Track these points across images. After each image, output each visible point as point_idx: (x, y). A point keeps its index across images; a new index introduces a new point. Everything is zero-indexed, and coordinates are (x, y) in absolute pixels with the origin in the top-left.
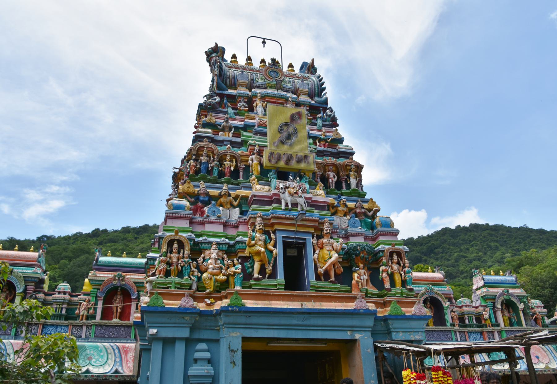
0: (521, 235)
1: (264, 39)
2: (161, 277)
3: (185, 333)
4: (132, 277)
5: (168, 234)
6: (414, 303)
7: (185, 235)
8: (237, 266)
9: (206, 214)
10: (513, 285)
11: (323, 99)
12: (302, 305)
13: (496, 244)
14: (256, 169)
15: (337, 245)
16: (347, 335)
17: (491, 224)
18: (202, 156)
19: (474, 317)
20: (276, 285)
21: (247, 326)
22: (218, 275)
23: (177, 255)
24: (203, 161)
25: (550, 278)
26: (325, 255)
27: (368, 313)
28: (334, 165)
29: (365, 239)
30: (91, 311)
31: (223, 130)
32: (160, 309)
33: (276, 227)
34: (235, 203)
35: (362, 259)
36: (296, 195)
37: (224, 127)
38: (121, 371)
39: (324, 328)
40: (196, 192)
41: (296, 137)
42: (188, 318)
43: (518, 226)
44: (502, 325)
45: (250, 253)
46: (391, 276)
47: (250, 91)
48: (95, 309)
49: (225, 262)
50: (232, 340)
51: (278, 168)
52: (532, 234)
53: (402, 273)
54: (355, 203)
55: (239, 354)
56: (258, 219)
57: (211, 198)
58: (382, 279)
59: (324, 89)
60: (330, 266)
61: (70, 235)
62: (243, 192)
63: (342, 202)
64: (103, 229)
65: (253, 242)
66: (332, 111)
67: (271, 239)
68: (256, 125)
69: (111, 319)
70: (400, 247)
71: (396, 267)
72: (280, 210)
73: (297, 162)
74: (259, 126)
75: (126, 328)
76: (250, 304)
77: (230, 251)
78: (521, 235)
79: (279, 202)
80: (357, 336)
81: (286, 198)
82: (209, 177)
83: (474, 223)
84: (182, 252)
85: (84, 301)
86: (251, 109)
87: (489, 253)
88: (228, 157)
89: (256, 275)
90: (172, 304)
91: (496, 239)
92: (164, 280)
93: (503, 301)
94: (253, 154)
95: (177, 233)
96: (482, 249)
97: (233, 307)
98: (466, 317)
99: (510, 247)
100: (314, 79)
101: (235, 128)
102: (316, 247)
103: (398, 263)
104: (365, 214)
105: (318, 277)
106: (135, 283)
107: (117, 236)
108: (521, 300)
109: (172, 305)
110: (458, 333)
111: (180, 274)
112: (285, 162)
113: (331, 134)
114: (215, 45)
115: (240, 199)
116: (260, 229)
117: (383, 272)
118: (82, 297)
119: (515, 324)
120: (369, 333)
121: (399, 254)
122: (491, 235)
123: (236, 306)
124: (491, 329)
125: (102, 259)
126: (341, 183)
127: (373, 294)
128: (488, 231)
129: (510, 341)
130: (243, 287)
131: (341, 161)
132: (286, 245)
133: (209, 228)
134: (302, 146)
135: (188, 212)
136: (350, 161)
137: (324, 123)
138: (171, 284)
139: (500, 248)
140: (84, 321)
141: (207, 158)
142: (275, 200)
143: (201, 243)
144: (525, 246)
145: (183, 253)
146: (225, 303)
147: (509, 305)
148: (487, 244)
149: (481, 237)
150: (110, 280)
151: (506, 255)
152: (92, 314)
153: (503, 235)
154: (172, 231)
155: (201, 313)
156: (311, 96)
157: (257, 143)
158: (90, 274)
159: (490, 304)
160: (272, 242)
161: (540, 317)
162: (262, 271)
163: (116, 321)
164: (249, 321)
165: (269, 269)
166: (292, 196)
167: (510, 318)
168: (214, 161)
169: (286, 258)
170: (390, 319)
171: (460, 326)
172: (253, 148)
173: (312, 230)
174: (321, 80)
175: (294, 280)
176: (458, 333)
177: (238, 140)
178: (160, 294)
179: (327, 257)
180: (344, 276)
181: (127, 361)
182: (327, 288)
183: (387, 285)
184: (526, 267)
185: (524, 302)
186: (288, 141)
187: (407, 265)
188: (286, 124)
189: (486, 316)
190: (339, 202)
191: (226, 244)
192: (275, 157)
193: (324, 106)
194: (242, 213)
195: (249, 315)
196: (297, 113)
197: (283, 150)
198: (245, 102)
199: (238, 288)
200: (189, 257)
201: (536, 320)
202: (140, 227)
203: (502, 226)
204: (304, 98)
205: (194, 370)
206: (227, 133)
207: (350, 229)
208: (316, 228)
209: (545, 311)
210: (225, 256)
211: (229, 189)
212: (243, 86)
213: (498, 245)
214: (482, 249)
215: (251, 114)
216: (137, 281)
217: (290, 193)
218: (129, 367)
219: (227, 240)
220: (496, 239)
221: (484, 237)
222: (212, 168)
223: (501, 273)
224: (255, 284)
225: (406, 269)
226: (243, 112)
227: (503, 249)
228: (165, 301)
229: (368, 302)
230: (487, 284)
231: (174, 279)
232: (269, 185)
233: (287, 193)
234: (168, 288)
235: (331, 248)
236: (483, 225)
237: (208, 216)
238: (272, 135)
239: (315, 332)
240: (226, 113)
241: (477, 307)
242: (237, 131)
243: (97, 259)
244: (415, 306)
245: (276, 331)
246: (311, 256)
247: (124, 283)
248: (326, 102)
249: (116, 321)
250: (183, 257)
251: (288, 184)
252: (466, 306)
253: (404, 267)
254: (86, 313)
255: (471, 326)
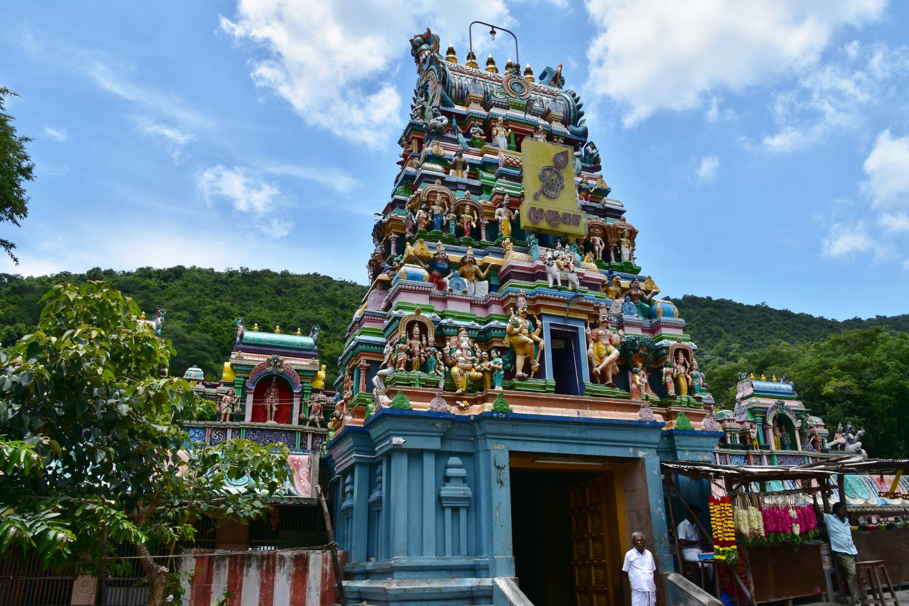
0: (757, 318)
1: (493, 27)
2: (402, 371)
3: (436, 444)
4: (292, 362)
5: (407, 313)
6: (703, 416)
7: (428, 315)
8: (496, 360)
9: (449, 288)
10: (787, 396)
11: (580, 129)
12: (578, 413)
13: (720, 328)
14: (506, 228)
15: (616, 337)
16: (629, 453)
17: (715, 298)
18: (434, 204)
19: (738, 436)
20: (544, 387)
21: (513, 437)
22: (470, 370)
23: (419, 342)
24: (436, 213)
25: (807, 385)
26: (600, 350)
27: (655, 426)
28: (602, 227)
29: (643, 331)
30: (237, 409)
31: (454, 167)
32: (406, 412)
33: (543, 311)
34: (483, 275)
35: (641, 355)
36: (567, 269)
37: (456, 163)
38: (295, 492)
39: (602, 443)
40: (432, 256)
41: (562, 187)
42: (439, 425)
43: (753, 303)
44: (773, 448)
45: (511, 344)
46: (676, 380)
47: (487, 110)
48: (243, 407)
49: (478, 354)
50: (499, 453)
51: (540, 229)
52: (772, 318)
53: (689, 376)
54: (629, 282)
55: (506, 473)
56: (521, 299)
57: (453, 266)
58: (666, 383)
59: (582, 114)
60: (607, 365)
61: (49, 276)
62: (492, 260)
63: (614, 279)
64: (107, 268)
65: (516, 330)
66: (594, 148)
67: (535, 326)
68: (501, 164)
69: (265, 421)
70: (687, 344)
71: (682, 369)
72: (545, 288)
73: (565, 223)
74: (504, 166)
75: (289, 434)
76: (518, 409)
77: (483, 339)
78: (757, 318)
79: (544, 277)
80: (641, 454)
81: (554, 271)
82: (445, 235)
83: (690, 294)
84: (424, 338)
85: (227, 394)
86: (490, 138)
87: (707, 341)
88: (468, 208)
89: (519, 373)
90: (421, 406)
91: (719, 320)
92: (404, 375)
93: (775, 417)
94: (501, 206)
95: (418, 312)
96: (698, 334)
97: (498, 413)
98: (729, 435)
99: (740, 335)
100: (568, 98)
101: (471, 165)
102: (590, 339)
103: (685, 365)
104: (641, 298)
105: (593, 378)
106: (297, 370)
107: (133, 282)
108: (798, 417)
109: (420, 407)
110: (717, 455)
111: (424, 367)
112: (549, 222)
113: (594, 182)
114: (426, 31)
115: (490, 269)
116: (524, 313)
117: (667, 373)
118: (222, 388)
119: (788, 446)
120: (655, 451)
121: (686, 352)
122: (714, 315)
123: (502, 412)
124: (757, 451)
125: (248, 335)
126: (609, 253)
127: (654, 402)
128: (709, 309)
129: (823, 466)
130: (504, 388)
131: (610, 222)
132: (554, 335)
133: (452, 306)
134: (568, 202)
135: (427, 283)
136: (622, 223)
137: (584, 164)
138: (414, 380)
139: (725, 334)
140: (228, 422)
141: (441, 208)
142: (537, 274)
143: (446, 326)
144: (761, 334)
145: (427, 339)
146: (488, 407)
147: (782, 422)
148: (706, 328)
149: (699, 317)
150: (262, 367)
151: (733, 345)
152: (238, 412)
153: (731, 315)
154: (412, 309)
155: (455, 420)
156: (565, 122)
157: (506, 191)
158: (233, 356)
159: (759, 419)
160: (538, 330)
161: (819, 439)
162: (527, 368)
163: (271, 423)
164: (516, 430)
165: (536, 364)
166: (562, 270)
167: (781, 439)
168: (449, 212)
169: (554, 351)
170: (677, 434)
171: (721, 447)
172: (501, 197)
173: (585, 317)
174: (577, 101)
175: (566, 382)
176: (717, 455)
177: (477, 183)
178: (405, 393)
179: (604, 352)
180: (622, 380)
181: (300, 479)
182: (604, 392)
183: (672, 392)
184: (773, 367)
185: (802, 419)
186: (552, 193)
187: (695, 367)
188: (549, 169)
189: (754, 435)
190: (610, 278)
191: (476, 330)
192: (536, 214)
193: (583, 139)
194: (491, 288)
195: (516, 423)
196: (562, 153)
197: (545, 204)
198: (480, 126)
199: (499, 388)
200: (435, 346)
201: (814, 442)
202: (170, 270)
203: (730, 302)
204: (557, 127)
205: (448, 490)
206: (460, 171)
207: (626, 317)
208: (590, 315)
209: (826, 431)
210: (476, 345)
211: (476, 254)
212: (476, 102)
213: (722, 330)
214: (698, 334)
215: (488, 146)
216: (300, 368)
217: (559, 266)
218: (303, 487)
219: (477, 325)
220: (719, 320)
221: (703, 317)
222: (448, 221)
223: (775, 379)
224: (519, 385)
225: (694, 372)
226: (478, 141)
227: (729, 336)
228: (411, 403)
229: (655, 413)
230: (758, 393)
231: (416, 373)
232: (526, 252)
233: (555, 266)
234: (410, 385)
235: (608, 342)
236: (703, 298)
237: (451, 290)
238: (531, 185)
239: (592, 448)
240: (456, 141)
241: (741, 423)
242: (474, 170)
243: (242, 335)
244: (705, 420)
245: (547, 445)
246: (587, 351)
247: (282, 370)
248: (585, 133)
249: (271, 423)
250: (427, 345)
251: (556, 253)
252: (729, 420)
253: (691, 369)
254: (230, 411)
255: (733, 447)
